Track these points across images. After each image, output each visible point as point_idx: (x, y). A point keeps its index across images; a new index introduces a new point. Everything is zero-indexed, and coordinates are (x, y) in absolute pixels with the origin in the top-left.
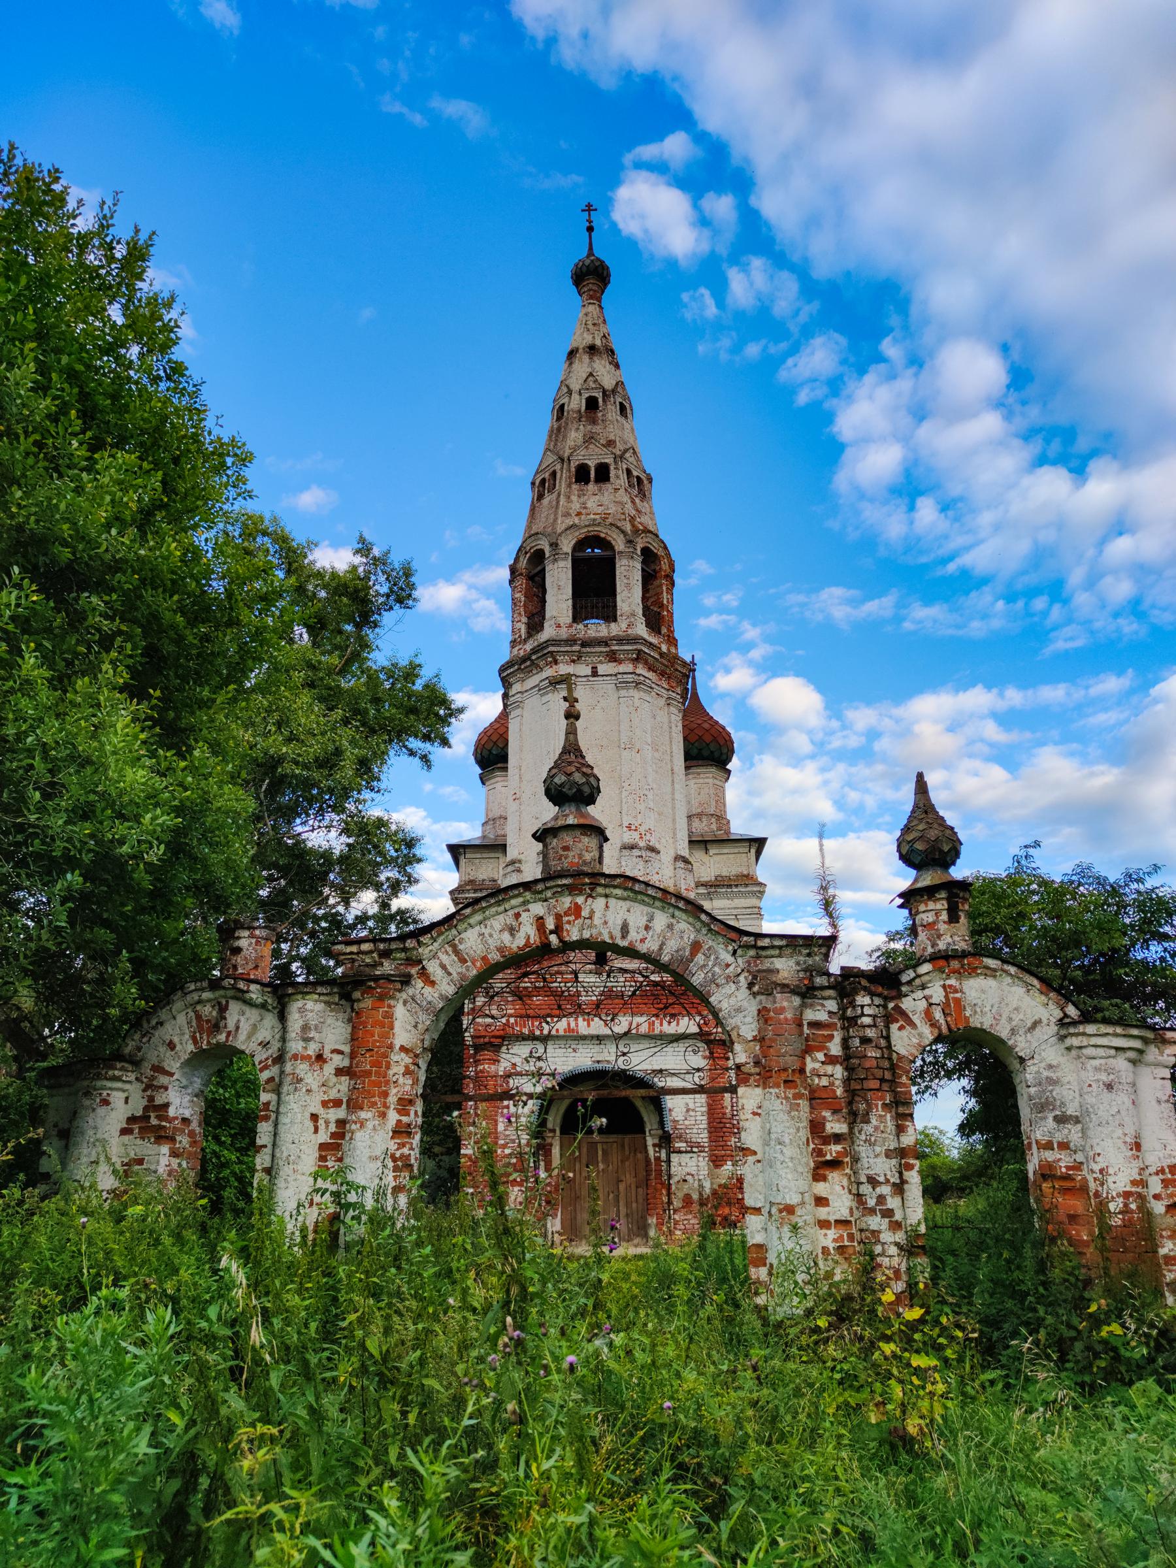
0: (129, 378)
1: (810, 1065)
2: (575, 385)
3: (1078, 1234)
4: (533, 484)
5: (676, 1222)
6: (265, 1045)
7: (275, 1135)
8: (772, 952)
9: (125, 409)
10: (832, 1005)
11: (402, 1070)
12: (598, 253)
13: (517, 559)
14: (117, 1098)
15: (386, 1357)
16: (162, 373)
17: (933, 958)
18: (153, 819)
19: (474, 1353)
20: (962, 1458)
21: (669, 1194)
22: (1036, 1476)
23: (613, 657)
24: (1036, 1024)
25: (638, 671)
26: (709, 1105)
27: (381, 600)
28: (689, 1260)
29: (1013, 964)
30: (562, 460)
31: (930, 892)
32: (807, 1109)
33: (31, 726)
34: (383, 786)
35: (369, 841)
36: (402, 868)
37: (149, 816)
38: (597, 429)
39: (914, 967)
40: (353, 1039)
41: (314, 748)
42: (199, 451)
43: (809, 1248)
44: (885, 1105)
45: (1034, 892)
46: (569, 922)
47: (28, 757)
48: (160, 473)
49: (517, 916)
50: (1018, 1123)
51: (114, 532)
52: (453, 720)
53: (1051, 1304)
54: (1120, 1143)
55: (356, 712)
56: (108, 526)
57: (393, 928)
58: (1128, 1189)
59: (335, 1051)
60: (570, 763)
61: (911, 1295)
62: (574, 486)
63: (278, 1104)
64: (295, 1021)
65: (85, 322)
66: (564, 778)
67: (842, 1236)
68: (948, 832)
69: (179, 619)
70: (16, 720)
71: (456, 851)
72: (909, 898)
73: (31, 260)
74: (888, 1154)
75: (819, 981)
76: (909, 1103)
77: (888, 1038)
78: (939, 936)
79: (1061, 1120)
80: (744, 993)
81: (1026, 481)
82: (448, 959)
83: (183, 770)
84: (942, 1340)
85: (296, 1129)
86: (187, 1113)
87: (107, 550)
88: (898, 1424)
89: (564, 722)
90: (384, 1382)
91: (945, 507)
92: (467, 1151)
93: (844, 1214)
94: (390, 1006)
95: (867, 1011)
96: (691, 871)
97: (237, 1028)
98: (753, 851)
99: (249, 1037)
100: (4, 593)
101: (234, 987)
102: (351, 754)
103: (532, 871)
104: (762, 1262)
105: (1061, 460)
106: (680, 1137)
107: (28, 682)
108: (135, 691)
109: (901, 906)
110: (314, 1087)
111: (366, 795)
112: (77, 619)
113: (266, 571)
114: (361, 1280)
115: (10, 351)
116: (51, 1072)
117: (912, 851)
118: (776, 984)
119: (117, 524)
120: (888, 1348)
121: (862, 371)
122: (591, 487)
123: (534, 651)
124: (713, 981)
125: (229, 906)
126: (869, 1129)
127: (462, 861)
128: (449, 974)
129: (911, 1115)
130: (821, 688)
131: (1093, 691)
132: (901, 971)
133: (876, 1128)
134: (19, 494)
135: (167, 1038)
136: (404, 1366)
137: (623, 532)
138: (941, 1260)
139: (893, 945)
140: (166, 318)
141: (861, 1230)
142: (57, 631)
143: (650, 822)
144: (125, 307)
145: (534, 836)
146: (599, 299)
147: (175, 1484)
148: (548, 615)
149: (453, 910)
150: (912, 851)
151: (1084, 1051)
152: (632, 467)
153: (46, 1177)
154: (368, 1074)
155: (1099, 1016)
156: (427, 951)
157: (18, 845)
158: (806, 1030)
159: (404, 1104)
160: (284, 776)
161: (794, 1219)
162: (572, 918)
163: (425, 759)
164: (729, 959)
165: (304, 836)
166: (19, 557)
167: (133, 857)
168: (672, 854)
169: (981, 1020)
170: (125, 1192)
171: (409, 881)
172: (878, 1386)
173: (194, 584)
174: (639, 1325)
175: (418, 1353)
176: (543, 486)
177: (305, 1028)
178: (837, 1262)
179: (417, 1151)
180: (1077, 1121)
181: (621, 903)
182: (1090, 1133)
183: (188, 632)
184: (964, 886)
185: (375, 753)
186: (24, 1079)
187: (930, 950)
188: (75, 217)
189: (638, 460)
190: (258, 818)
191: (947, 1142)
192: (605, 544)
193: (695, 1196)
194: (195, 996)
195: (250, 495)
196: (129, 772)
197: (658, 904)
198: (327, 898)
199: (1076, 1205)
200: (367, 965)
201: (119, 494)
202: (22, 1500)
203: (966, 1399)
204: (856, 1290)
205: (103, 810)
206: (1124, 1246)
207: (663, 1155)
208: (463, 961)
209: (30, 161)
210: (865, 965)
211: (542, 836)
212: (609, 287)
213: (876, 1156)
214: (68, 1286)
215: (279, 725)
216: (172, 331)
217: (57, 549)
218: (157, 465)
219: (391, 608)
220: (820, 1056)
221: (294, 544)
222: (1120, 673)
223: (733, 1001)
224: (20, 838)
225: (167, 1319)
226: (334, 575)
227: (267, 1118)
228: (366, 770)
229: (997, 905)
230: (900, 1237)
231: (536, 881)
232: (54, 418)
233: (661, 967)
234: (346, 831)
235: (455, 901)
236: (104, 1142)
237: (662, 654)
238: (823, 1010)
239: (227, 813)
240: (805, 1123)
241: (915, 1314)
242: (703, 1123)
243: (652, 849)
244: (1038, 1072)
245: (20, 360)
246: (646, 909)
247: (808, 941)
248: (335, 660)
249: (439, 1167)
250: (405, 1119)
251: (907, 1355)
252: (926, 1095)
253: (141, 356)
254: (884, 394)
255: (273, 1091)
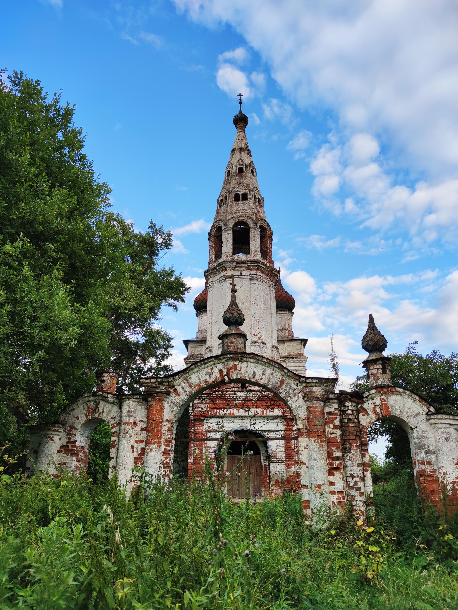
0: (65, 160)
1: (327, 429)
2: (234, 163)
3: (435, 498)
4: (218, 201)
5: (272, 490)
6: (113, 418)
7: (117, 453)
8: (312, 384)
9: (63, 172)
10: (336, 406)
11: (167, 429)
12: (243, 112)
13: (211, 230)
14: (56, 438)
15: (165, 545)
16: (77, 158)
17: (376, 387)
18: (74, 330)
19: (199, 545)
20: (390, 589)
21: (269, 479)
22: (419, 596)
23: (248, 268)
24: (417, 414)
25: (258, 274)
26: (285, 444)
27: (159, 246)
28: (281, 507)
29: (408, 390)
30: (229, 192)
31: (375, 361)
32: (326, 447)
33: (26, 294)
34: (159, 317)
35: (154, 339)
36: (166, 350)
37: (71, 329)
38: (243, 180)
39: (369, 391)
40: (148, 416)
41: (133, 303)
42: (91, 188)
43: (326, 502)
44: (357, 446)
45: (415, 362)
46: (232, 372)
47: (25, 306)
48: (76, 197)
49: (212, 369)
50: (410, 453)
51: (59, 219)
52: (186, 292)
53: (423, 526)
54: (451, 462)
55: (149, 289)
56: (57, 217)
57: (162, 373)
58: (455, 480)
59: (141, 421)
60: (233, 309)
61: (368, 522)
62: (234, 202)
63: (119, 441)
64: (125, 409)
65: (48, 139)
66: (230, 315)
67: (340, 498)
68: (382, 338)
69: (83, 253)
70: (21, 291)
71: (187, 343)
72: (367, 364)
73: (28, 115)
74: (358, 465)
75: (331, 396)
76: (367, 445)
77: (358, 419)
78: (378, 379)
79: (428, 452)
80: (301, 400)
81: (390, 192)
82: (185, 385)
83: (84, 311)
84: (381, 540)
85: (125, 451)
86: (83, 445)
87: (56, 226)
88: (364, 573)
89: (230, 294)
90: (163, 554)
91: (358, 201)
92: (191, 460)
93: (341, 489)
94: (162, 404)
95: (350, 408)
96: (278, 352)
97: (103, 411)
98: (302, 344)
99: (108, 415)
100: (17, 243)
101: (102, 395)
102: (147, 305)
103: (217, 351)
104: (308, 507)
105: (403, 183)
106: (274, 457)
107: (25, 277)
108: (66, 281)
109: (363, 367)
110: (133, 435)
111: (153, 321)
112: (44, 253)
113: (116, 234)
114: (155, 514)
115: (20, 150)
116: (31, 428)
117: (368, 345)
118: (314, 397)
119: (60, 216)
120: (360, 543)
121: (319, 147)
122: (240, 202)
123: (218, 265)
124: (289, 396)
125: (100, 364)
126: (350, 455)
127: (189, 347)
128: (185, 391)
129: (367, 450)
130: (312, 274)
131: (423, 278)
132: (364, 393)
133: (354, 455)
134: (23, 205)
135: (76, 415)
136: (172, 549)
137: (252, 220)
138: (379, 508)
139: (359, 382)
140: (79, 138)
141: (348, 495)
142: (36, 257)
143: (262, 332)
144: (64, 134)
145: (218, 337)
146: (244, 130)
147: (83, 596)
148: (223, 252)
149: (185, 366)
150: (368, 345)
151: (437, 425)
152: (256, 195)
153: (29, 468)
154: (154, 430)
155: (442, 411)
156: (177, 382)
157: (20, 340)
158: (326, 415)
159: (168, 442)
160: (121, 314)
161: (321, 490)
162: (233, 370)
163: (175, 307)
164: (295, 387)
165: (128, 337)
166: (22, 229)
167: (64, 345)
168: (271, 345)
169: (395, 412)
170: (60, 476)
171: (168, 355)
172: (356, 558)
173: (89, 239)
174: (261, 532)
175: (178, 544)
176: (222, 202)
177: (129, 412)
178: (338, 508)
179: (172, 461)
180: (434, 453)
181: (252, 364)
182: (440, 458)
183: (86, 258)
184: (388, 359)
185: (156, 305)
186: (20, 430)
187: (375, 384)
188: (45, 99)
189: (259, 192)
190: (111, 330)
191: (379, 460)
192: (246, 224)
193: (280, 480)
194: (87, 399)
195: (110, 205)
196: (64, 313)
197: (267, 365)
198: (137, 361)
199: (434, 487)
200: (154, 387)
201: (61, 205)
202: (25, 602)
203: (391, 564)
204: (345, 519)
205: (53, 327)
206: (453, 503)
207: (267, 464)
208: (191, 386)
209: (28, 78)
210: (349, 389)
211: (222, 337)
212: (248, 125)
213: (354, 466)
214: (38, 513)
215: (120, 294)
216: (81, 142)
217: (37, 226)
218: (75, 194)
219: (163, 249)
220: (331, 426)
221: (126, 224)
222: (433, 270)
223: (297, 403)
224: (21, 337)
225: (80, 529)
226: (141, 236)
227: (114, 447)
228: (153, 312)
229: (400, 367)
230: (363, 498)
231: (219, 356)
232: (37, 176)
233: (269, 390)
234: (145, 335)
235: (186, 363)
236: (51, 456)
237: (267, 267)
238: (332, 408)
239: (100, 328)
240: (325, 452)
241: (370, 530)
242: (283, 451)
243: (263, 343)
244: (418, 433)
245: (24, 154)
246: (262, 367)
247: (326, 380)
248: (141, 269)
249: (180, 466)
250: (168, 448)
251: (367, 546)
252: (373, 441)
253: (69, 152)
254: (329, 156)
255: (116, 436)
